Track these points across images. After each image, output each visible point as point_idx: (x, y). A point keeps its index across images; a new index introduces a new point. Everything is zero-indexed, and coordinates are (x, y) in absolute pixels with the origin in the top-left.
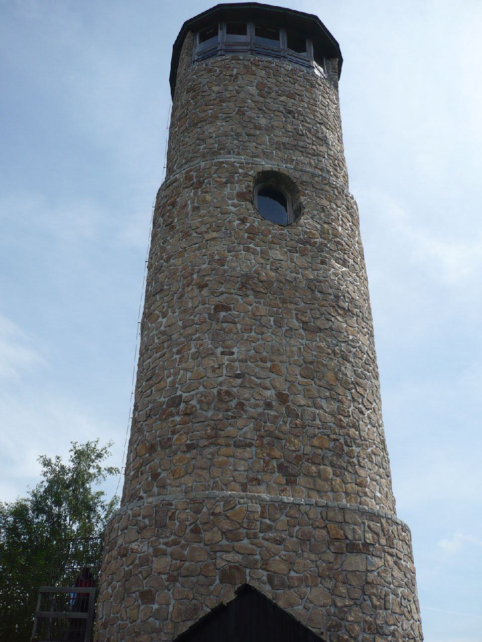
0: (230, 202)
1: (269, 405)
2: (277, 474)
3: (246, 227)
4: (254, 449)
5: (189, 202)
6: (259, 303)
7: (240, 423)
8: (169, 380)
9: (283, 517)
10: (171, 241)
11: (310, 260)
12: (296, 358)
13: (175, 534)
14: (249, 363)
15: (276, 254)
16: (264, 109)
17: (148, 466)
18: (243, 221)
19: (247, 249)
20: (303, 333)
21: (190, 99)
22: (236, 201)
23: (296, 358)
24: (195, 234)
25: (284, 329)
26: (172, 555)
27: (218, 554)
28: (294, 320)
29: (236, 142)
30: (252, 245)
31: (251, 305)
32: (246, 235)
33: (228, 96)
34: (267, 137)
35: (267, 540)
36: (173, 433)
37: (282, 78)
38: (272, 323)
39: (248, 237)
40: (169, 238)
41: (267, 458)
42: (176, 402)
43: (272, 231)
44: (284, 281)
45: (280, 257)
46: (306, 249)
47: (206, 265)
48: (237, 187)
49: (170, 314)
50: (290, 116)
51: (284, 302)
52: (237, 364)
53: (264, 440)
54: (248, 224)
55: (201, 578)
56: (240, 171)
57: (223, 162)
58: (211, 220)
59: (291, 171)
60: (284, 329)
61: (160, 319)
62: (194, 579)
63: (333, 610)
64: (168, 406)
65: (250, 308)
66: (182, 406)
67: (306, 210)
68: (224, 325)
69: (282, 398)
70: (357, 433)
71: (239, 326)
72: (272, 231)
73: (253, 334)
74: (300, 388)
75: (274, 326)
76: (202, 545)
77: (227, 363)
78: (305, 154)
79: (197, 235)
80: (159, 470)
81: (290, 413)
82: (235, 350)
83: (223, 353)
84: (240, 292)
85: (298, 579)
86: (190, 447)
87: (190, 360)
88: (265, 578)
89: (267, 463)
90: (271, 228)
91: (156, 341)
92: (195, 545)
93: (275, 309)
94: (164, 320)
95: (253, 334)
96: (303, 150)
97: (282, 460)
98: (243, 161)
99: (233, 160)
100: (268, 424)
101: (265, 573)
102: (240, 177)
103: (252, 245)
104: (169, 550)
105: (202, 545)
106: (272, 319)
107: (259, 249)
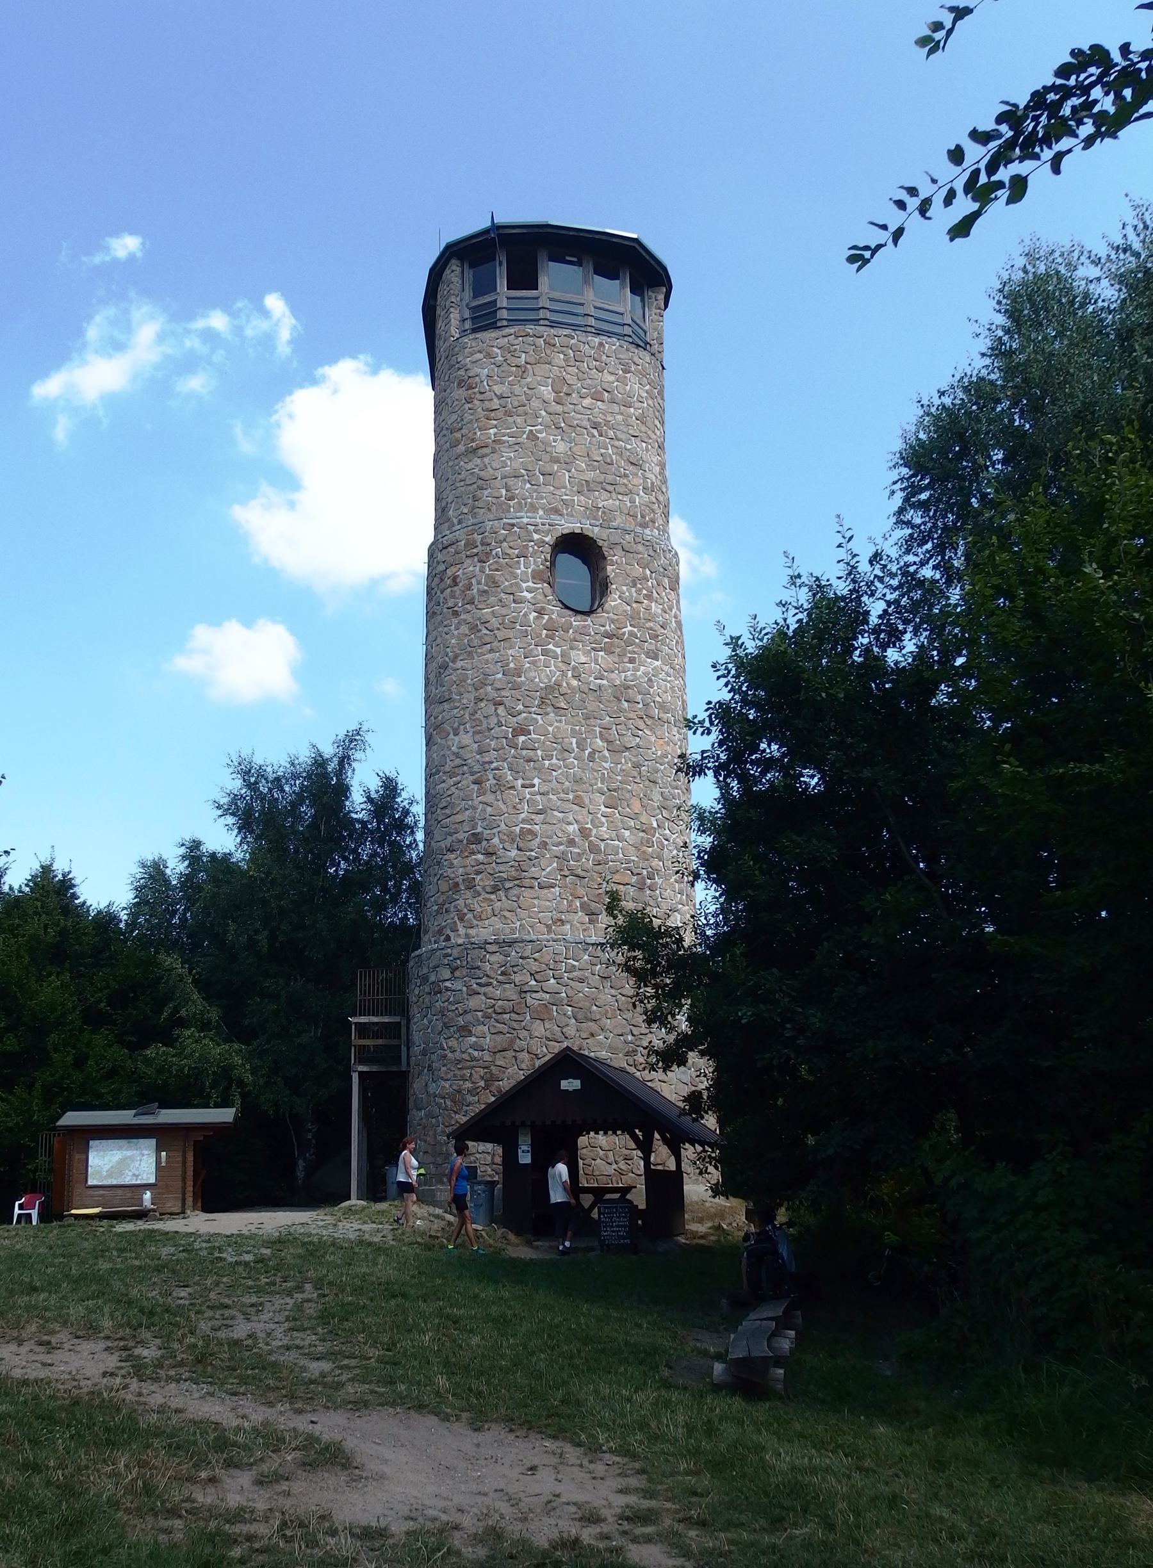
0: (524, 585)
1: (571, 843)
2: (580, 913)
3: (544, 621)
4: (557, 889)
5: (474, 581)
6: (560, 721)
7: (543, 863)
8: (467, 813)
9: (586, 957)
10: (456, 633)
11: (616, 660)
12: (599, 785)
13: (488, 976)
14: (551, 796)
15: (579, 657)
16: (563, 425)
17: (453, 904)
18: (540, 613)
19: (545, 653)
20: (607, 755)
21: (464, 401)
22: (530, 584)
23: (599, 785)
24: (485, 631)
25: (587, 752)
26: (485, 994)
27: (528, 994)
28: (598, 740)
29: (528, 486)
30: (551, 646)
31: (551, 725)
32: (545, 631)
33: (516, 404)
34: (567, 474)
35: (572, 979)
36: (478, 873)
37: (585, 364)
38: (574, 745)
39: (547, 636)
40: (453, 627)
41: (570, 898)
42: (476, 839)
43: (574, 623)
44: (586, 691)
45: (583, 659)
46: (612, 645)
47: (500, 676)
48: (532, 563)
49: (462, 732)
50: (595, 432)
51: (587, 718)
52: (538, 797)
53: (568, 879)
54: (546, 617)
55: (512, 1015)
56: (536, 537)
57: (513, 525)
58: (504, 611)
59: (596, 529)
60: (587, 752)
61: (451, 736)
62: (507, 1016)
63: (630, 1038)
64: (470, 843)
65: (550, 729)
66: (484, 843)
67: (614, 586)
68: (524, 752)
69: (584, 833)
70: (661, 863)
71: (539, 752)
72: (574, 623)
73: (554, 761)
74: (603, 819)
75: (576, 750)
76: (513, 985)
77: (528, 796)
78: (614, 495)
79: (488, 632)
80: (465, 911)
81: (594, 849)
82: (536, 781)
83: (523, 786)
84: (539, 711)
85: (600, 1013)
86: (495, 890)
87: (489, 792)
88: (569, 1013)
89: (570, 904)
90: (572, 619)
91: (449, 763)
92: (507, 986)
93: (577, 728)
94: (457, 738)
95: (554, 761)
96: (611, 488)
97: (586, 899)
98: (539, 520)
99: (525, 520)
100: (572, 862)
101: (570, 1008)
102: (536, 548)
103: (551, 646)
104: (483, 990)
105: (513, 985)
106: (574, 740)
107: (558, 650)
